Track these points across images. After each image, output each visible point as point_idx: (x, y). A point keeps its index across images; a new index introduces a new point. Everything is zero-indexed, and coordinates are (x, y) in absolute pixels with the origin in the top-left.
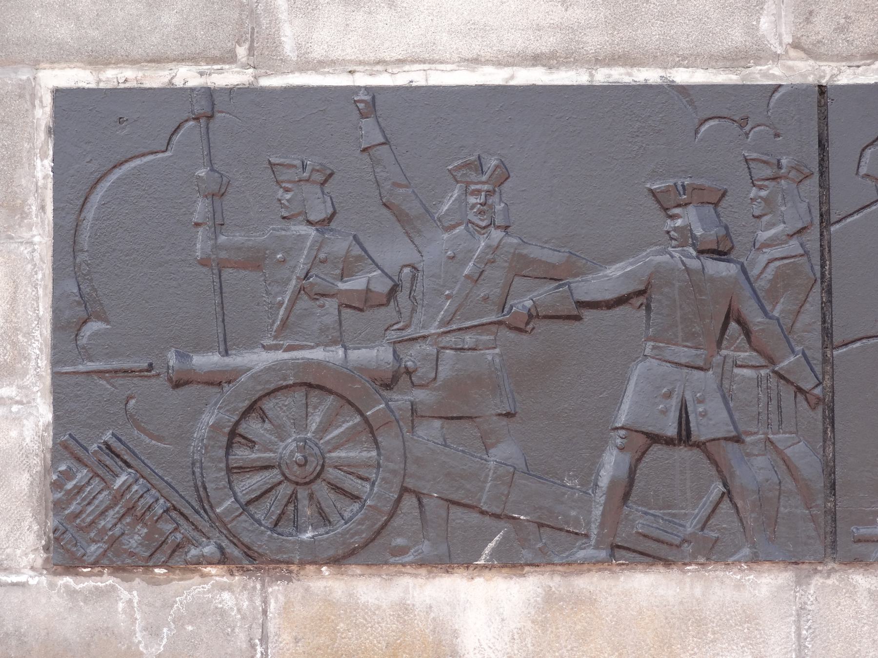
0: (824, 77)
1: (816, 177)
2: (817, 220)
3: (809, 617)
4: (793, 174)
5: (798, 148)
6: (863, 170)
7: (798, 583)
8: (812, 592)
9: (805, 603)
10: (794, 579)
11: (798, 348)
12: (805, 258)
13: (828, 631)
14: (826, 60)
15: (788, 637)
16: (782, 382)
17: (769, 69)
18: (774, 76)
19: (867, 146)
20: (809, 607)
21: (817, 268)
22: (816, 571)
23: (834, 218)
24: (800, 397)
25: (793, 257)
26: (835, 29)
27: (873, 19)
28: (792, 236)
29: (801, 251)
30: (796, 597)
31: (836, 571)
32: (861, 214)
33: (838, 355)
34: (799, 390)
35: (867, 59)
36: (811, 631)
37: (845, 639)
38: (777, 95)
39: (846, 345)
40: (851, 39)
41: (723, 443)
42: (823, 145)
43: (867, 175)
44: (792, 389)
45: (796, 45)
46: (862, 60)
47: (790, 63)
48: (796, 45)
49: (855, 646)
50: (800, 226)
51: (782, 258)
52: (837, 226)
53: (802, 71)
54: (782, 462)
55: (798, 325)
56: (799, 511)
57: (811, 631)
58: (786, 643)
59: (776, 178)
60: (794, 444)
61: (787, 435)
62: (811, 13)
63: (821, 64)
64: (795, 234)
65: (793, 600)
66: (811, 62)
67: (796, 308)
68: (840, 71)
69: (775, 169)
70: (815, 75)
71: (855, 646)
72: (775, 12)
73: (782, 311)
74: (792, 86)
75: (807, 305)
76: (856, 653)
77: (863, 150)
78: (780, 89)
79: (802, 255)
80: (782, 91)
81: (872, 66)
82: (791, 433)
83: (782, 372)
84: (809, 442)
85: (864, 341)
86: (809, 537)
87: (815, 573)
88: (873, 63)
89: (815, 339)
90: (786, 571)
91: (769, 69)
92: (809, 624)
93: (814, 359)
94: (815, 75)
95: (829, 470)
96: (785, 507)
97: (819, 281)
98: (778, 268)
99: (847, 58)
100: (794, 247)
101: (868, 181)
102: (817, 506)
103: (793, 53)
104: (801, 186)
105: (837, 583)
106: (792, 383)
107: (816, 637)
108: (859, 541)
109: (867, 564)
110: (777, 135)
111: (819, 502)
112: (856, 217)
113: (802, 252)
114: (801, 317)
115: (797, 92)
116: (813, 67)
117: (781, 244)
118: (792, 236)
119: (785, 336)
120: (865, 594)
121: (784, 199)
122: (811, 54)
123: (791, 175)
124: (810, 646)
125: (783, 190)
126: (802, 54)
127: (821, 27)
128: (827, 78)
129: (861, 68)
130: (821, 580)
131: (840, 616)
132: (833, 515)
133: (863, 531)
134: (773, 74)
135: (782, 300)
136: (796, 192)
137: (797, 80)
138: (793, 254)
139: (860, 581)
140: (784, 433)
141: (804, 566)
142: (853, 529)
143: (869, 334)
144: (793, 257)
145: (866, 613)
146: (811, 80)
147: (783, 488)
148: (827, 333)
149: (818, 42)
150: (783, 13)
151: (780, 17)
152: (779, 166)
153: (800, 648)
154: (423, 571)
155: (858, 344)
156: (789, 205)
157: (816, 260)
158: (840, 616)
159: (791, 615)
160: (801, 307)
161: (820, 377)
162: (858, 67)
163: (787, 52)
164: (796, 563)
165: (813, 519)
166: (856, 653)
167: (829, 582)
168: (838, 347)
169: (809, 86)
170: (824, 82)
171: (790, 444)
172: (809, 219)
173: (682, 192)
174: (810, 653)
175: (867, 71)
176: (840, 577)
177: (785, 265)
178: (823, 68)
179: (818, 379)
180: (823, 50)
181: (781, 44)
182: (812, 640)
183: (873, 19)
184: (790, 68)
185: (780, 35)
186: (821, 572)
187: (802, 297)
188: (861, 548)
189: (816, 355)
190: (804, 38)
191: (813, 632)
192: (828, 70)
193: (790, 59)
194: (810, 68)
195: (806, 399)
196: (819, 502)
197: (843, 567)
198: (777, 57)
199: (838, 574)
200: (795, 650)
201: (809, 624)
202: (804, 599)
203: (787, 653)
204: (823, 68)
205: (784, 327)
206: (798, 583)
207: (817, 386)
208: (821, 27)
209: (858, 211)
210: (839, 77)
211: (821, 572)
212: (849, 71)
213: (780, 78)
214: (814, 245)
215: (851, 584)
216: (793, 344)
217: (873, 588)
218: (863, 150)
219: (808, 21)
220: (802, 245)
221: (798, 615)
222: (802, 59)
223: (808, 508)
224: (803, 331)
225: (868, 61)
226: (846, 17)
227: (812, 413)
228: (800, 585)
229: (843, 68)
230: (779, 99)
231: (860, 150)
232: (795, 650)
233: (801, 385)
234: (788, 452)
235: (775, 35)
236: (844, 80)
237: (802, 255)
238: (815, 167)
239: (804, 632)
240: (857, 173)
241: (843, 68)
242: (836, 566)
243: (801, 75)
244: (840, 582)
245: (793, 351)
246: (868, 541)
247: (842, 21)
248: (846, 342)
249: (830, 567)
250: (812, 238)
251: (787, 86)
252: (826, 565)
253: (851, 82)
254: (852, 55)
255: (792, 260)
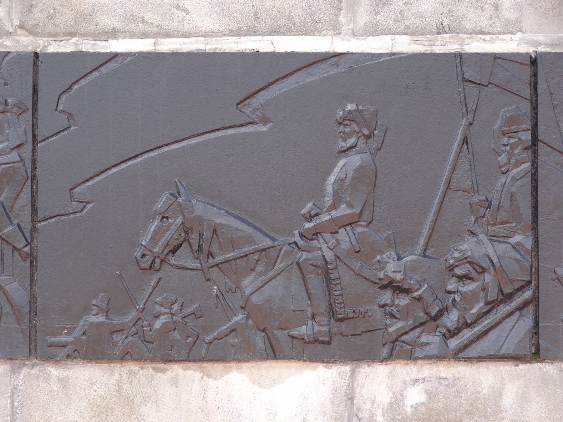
0: (39, 47)
1: (30, 112)
2: (30, 140)
3: (20, 394)
4: (15, 109)
5: (19, 93)
6: (60, 108)
7: (13, 371)
8: (22, 378)
9: (17, 385)
10: (10, 369)
11: (15, 222)
12: (21, 164)
13: (32, 403)
14: (40, 37)
15: (5, 407)
16: (5, 243)
17: (4, 41)
18: (6, 46)
19: (63, 92)
20: (20, 388)
21: (29, 170)
22: (24, 365)
23: (40, 138)
24: (16, 253)
25: (13, 163)
26: (47, 17)
27: (71, 11)
28: (13, 149)
29: (19, 159)
30: (11, 381)
31: (38, 365)
32: (58, 136)
33: (40, 226)
34: (15, 248)
35: (67, 36)
36: (21, 403)
37: (43, 408)
38: (7, 59)
39: (46, 220)
40: (57, 23)
41: (36, 287)
42: (35, 90)
43: (62, 111)
44: (11, 248)
45: (22, 26)
46: (63, 37)
47: (17, 38)
48: (22, 26)
49: (48, 413)
50: (18, 142)
51: (6, 164)
52: (43, 143)
53: (25, 43)
54: (3, 294)
55: (16, 206)
56: (13, 326)
57: (21, 403)
58: (4, 410)
59: (4, 112)
60: (11, 283)
61: (7, 277)
62: (32, 6)
63: (37, 39)
64: (14, 148)
65: (9, 383)
66: (31, 37)
67: (15, 195)
68: (49, 44)
69: (4, 106)
70: (33, 46)
71: (48, 413)
72: (8, 5)
73: (5, 197)
74: (17, 53)
75: (22, 194)
76: (49, 417)
77: (61, 95)
78: (9, 55)
79: (19, 162)
80: (10, 56)
81: (70, 41)
82: (9, 276)
83: (4, 237)
84: (21, 282)
85: (58, 217)
86: (19, 343)
87: (24, 366)
88: (70, 39)
89: (26, 216)
90: (5, 364)
91: (4, 41)
92: (19, 398)
93: (26, 228)
94: (33, 46)
95: (33, 299)
96: (5, 323)
97: (30, 179)
98: (3, 169)
99: (54, 35)
100: (14, 156)
101: (63, 115)
102: (24, 323)
103: (19, 31)
104: (20, 117)
105: (38, 373)
106: (10, 244)
107: (23, 406)
108: (50, 346)
109: (57, 361)
110: (6, 84)
111: (26, 320)
112: (55, 138)
113: (19, 160)
114: (18, 201)
115: (20, 57)
116: (32, 41)
117: (6, 154)
118: (13, 149)
119: (6, 213)
120: (56, 380)
121: (9, 125)
122: (31, 32)
123: (14, 110)
124: (20, 413)
125: (8, 119)
126: (26, 33)
127: (38, 16)
128: (41, 48)
129: (63, 42)
130: (28, 371)
131: (39, 394)
132: (32, 328)
133: (53, 339)
134: (6, 45)
135: (6, 190)
136: (17, 121)
137: (21, 49)
138: (13, 161)
139: (53, 372)
140: (5, 275)
141: (17, 361)
142: (47, 338)
143: (61, 213)
144: (13, 163)
145: (56, 392)
146: (30, 49)
147: (3, 311)
148: (34, 211)
149: (36, 25)
150: (14, 6)
151: (12, 8)
152: (6, 104)
153: (13, 414)
154: (69, 362)
155: (54, 220)
156: (12, 129)
157: (29, 165)
158: (39, 394)
159: (8, 393)
160: (18, 195)
161: (29, 240)
162: (61, 41)
163: (16, 31)
164: (12, 359)
165: (22, 331)
166: (49, 417)
167: (33, 372)
168: (41, 221)
169: (27, 53)
170: (38, 51)
171: (8, 283)
172: (25, 139)
173: (178, 183)
174: (19, 417)
175: (66, 43)
176: (40, 368)
177: (7, 168)
178: (38, 42)
179: (27, 241)
180: (38, 30)
181: (12, 25)
182: (21, 408)
183: (71, 11)
184: (17, 41)
185: (12, 20)
186: (27, 365)
187: (18, 188)
188: (53, 350)
189: (27, 227)
190: (27, 22)
191: (22, 404)
192: (41, 43)
193: (18, 35)
194: (30, 41)
195: (20, 254)
196: (26, 320)
197: (42, 362)
198: (8, 34)
199: (39, 367)
200: (10, 415)
201: (19, 398)
202: (17, 382)
203: (4, 417)
204: (38, 42)
205: (6, 208)
206: (13, 371)
207: (26, 246)
208: (38, 16)
209: (56, 134)
210: (48, 48)
211: (27, 365)
212: (55, 44)
213: (10, 47)
214: (27, 156)
215: (47, 373)
216: (12, 219)
217: (61, 376)
218: (61, 95)
219: (29, 11)
220: (19, 155)
221: (12, 392)
222: (25, 36)
223: (20, 324)
224: (19, 211)
225: (68, 38)
226: (55, 9)
227: (23, 264)
228: (14, 374)
229: (51, 42)
230: (8, 61)
231: (59, 94)
232: (10, 415)
233: (16, 245)
234: (7, 288)
235: (8, 20)
236: (51, 49)
237: (19, 162)
238: (30, 105)
239: (16, 404)
240: (56, 110)
241: (51, 42)
242: (37, 361)
243: (24, 45)
244: (40, 372)
245: (11, 223)
246: (57, 346)
247: (52, 12)
248: (46, 218)
249: (33, 362)
250: (27, 151)
251: (14, 52)
252: (31, 360)
253: (55, 51)
254: (57, 33)
255: (12, 165)
